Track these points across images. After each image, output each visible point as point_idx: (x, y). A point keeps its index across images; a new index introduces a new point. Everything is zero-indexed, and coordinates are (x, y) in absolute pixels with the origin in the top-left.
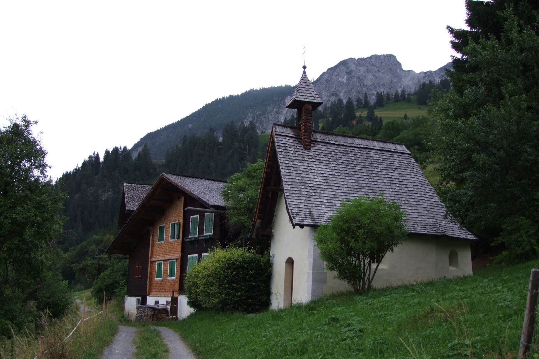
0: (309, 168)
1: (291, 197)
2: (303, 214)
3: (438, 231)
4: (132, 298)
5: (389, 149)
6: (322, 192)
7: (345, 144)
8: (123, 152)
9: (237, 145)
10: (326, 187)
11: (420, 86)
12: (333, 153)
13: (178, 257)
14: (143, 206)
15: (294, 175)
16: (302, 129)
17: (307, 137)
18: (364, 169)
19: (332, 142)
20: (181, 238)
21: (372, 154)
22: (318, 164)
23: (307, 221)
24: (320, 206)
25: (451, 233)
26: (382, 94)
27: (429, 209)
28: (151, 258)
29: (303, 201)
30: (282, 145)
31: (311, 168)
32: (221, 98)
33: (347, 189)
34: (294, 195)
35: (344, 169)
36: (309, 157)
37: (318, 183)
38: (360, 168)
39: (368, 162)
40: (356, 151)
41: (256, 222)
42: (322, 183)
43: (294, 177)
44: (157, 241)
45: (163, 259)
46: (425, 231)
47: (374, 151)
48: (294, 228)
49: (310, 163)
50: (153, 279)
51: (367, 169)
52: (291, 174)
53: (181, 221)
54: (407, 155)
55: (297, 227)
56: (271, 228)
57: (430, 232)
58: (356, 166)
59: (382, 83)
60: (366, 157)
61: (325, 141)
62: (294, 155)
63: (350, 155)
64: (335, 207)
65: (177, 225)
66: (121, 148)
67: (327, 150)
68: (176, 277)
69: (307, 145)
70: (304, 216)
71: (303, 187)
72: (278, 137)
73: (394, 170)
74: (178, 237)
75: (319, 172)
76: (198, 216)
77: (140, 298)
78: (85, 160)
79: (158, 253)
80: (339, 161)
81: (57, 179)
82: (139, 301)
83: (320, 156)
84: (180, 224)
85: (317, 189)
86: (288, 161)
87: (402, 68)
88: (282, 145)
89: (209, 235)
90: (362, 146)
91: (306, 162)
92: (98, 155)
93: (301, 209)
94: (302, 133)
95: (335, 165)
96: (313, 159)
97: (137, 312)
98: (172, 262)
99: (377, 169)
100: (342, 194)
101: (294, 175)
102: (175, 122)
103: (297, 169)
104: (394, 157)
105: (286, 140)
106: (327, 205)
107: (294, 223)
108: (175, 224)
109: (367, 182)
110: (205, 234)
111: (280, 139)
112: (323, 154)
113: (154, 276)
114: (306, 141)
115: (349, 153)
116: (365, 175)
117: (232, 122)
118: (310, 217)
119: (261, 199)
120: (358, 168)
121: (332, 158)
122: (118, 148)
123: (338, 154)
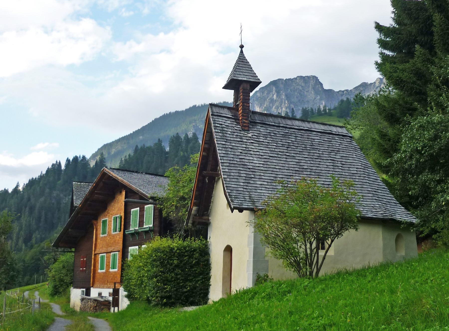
0: (247, 149)
1: (228, 180)
2: (242, 197)
3: (385, 215)
4: (78, 290)
5: (330, 132)
6: (262, 174)
7: (285, 126)
8: (82, 160)
9: (182, 153)
10: (266, 169)
11: (339, 102)
12: (273, 134)
13: (120, 250)
14: (86, 201)
15: (232, 156)
16: (240, 109)
17: (245, 118)
18: (305, 151)
19: (271, 123)
20: (122, 230)
21: (313, 136)
22: (257, 145)
23: (247, 204)
24: (260, 188)
25: (398, 217)
26: (307, 109)
27: (374, 193)
28: (95, 251)
29: (242, 184)
30: (219, 125)
31: (250, 149)
32: (168, 113)
33: (288, 171)
34: (232, 177)
35: (285, 151)
36: (248, 138)
37: (258, 165)
38: (301, 150)
39: (309, 144)
40: (297, 133)
41: (192, 209)
42: (262, 165)
43: (232, 159)
44: (100, 235)
45: (106, 252)
46: (372, 215)
47: (315, 133)
48: (232, 212)
49: (249, 144)
50: (97, 272)
51: (309, 151)
52: (229, 156)
53: (123, 214)
54: (349, 138)
55: (236, 211)
56: (208, 216)
57: (377, 216)
58: (297, 148)
59: (307, 100)
60: (306, 139)
61: (264, 122)
62: (231, 136)
63: (290, 137)
64: (276, 190)
65: (119, 218)
66: (80, 157)
67: (265, 131)
68: (118, 269)
69: (245, 126)
70: (243, 199)
71: (242, 169)
72: (215, 117)
73: (336, 152)
74: (119, 230)
75: (258, 153)
76: (138, 208)
77: (84, 290)
78: (49, 168)
79: (101, 246)
80: (279, 143)
81: (24, 184)
82: (84, 293)
83: (259, 137)
84: (121, 217)
85: (256, 171)
86: (225, 141)
87: (324, 87)
88: (219, 125)
89: (149, 227)
90: (303, 128)
91: (245, 143)
92: (60, 163)
93: (240, 192)
94: (240, 114)
95: (275, 147)
96: (252, 140)
97: (81, 303)
98: (114, 254)
99: (319, 151)
100: (284, 176)
101: (232, 156)
102: (128, 134)
103: (235, 151)
104: (335, 139)
105: (223, 121)
106: (268, 188)
107: (232, 207)
108: (117, 217)
109: (309, 165)
110: (145, 227)
111: (216, 119)
112: (262, 135)
113: (97, 268)
114: (244, 121)
115: (289, 134)
116: (307, 157)
117: (177, 134)
118: (249, 200)
119: (197, 184)
120: (299, 150)
121: (271, 139)
122: (78, 157)
123: (277, 135)
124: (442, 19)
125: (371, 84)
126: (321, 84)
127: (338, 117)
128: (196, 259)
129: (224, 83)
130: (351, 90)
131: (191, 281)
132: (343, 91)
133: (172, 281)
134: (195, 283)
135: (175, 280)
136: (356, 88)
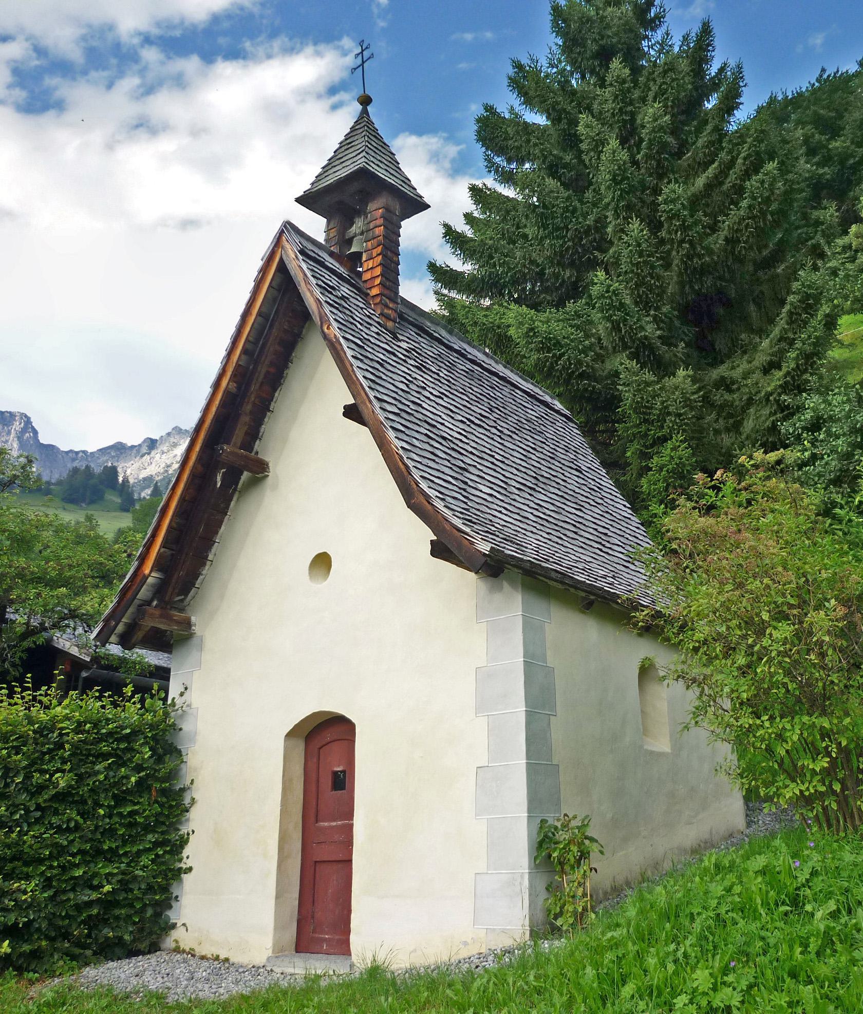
124: (642, 230)
125: (133, 447)
126: (35, 432)
127: (63, 500)
128: (139, 768)
129: (303, 185)
130: (91, 453)
131: (112, 856)
132: (77, 453)
133: (41, 861)
134: (128, 865)
135: (51, 857)
136: (103, 451)
